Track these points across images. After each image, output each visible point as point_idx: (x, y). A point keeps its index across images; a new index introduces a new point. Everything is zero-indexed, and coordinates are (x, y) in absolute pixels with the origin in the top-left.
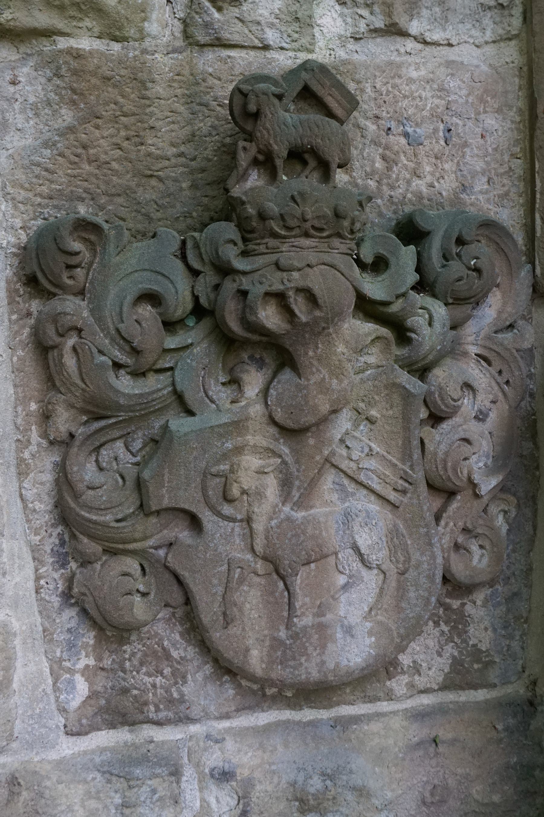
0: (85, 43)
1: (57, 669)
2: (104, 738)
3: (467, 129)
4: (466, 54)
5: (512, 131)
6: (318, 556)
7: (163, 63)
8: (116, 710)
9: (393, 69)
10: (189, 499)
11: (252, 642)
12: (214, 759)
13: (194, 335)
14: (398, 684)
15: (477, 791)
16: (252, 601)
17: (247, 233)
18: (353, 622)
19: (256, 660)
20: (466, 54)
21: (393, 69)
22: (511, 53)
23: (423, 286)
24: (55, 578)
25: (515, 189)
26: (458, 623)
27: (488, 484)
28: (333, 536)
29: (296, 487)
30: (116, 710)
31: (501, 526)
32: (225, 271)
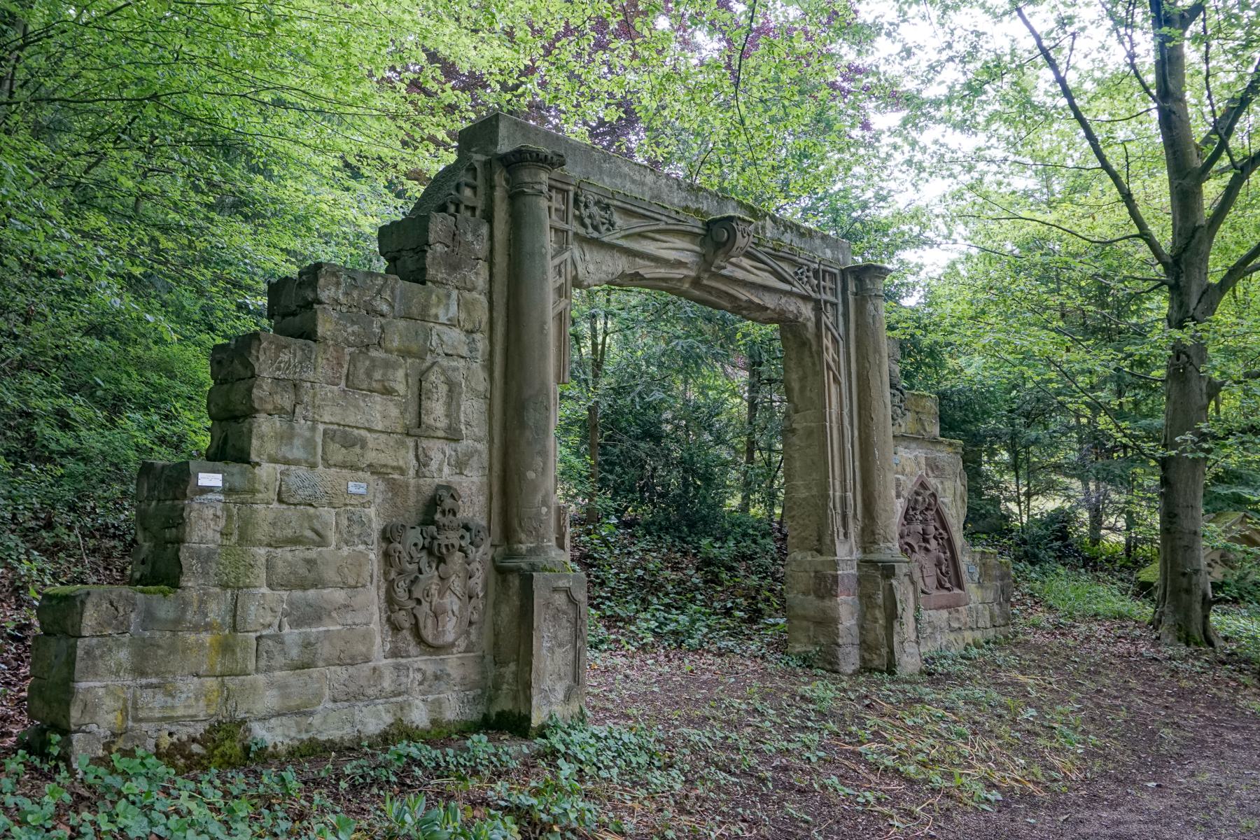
0: (396, 476)
1: (383, 640)
2: (390, 661)
3: (475, 499)
4: (475, 479)
5: (885, 538)
6: (445, 612)
7: (412, 481)
8: (395, 653)
9: (460, 483)
10: (420, 596)
11: (428, 633)
12: (416, 666)
13: (424, 554)
14: (455, 650)
15: (473, 676)
16: (430, 622)
17: (438, 528)
18: (450, 630)
19: (430, 639)
20: (475, 479)
21: (460, 483)
22: (485, 479)
23: (471, 543)
24: (384, 617)
25: (485, 515)
26: (468, 633)
27: (481, 595)
28: (449, 607)
29: (441, 594)
30: (395, 653)
31: (937, 393)
32: (433, 538)
